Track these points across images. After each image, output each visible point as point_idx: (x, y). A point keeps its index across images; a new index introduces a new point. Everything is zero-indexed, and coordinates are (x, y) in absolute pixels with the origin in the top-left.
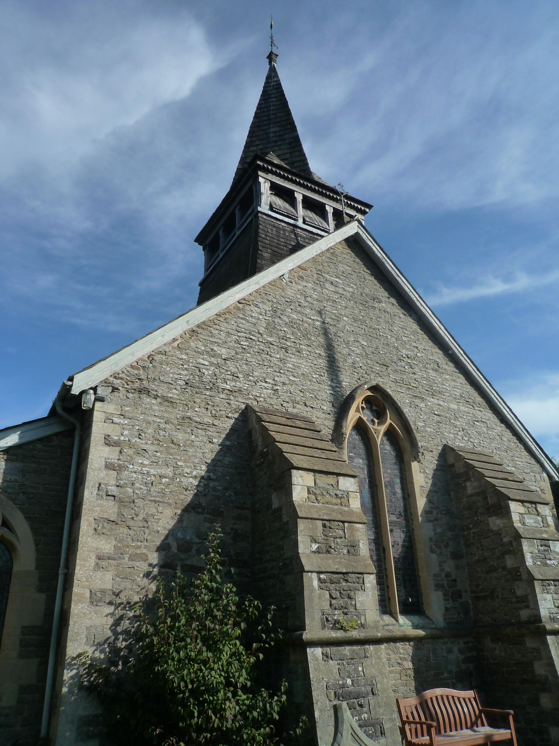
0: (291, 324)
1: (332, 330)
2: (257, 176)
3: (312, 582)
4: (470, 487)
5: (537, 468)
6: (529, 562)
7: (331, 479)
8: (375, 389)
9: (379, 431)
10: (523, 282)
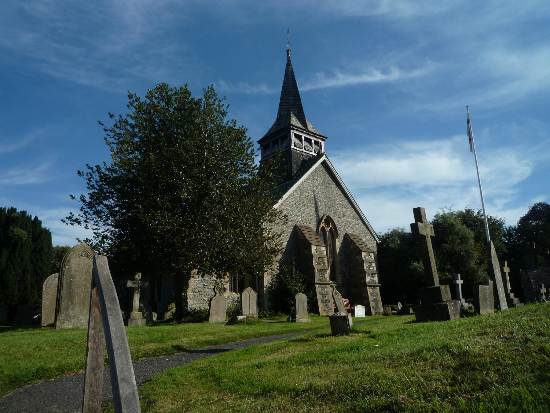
0: (306, 197)
1: (316, 197)
2: (290, 132)
3: (316, 271)
5: (373, 239)
6: (365, 268)
7: (319, 247)
8: (328, 217)
9: (328, 229)
10: (395, 75)
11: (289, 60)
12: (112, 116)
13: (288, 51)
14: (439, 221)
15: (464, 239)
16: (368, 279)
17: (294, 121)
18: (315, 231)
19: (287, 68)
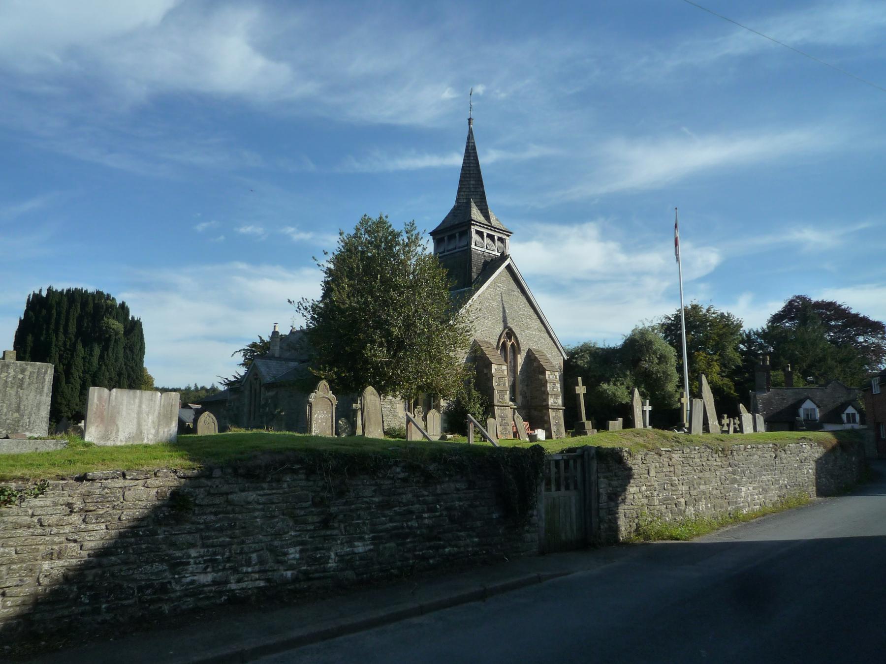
3: (496, 392)
4: (535, 364)
9: (509, 344)
11: (471, 131)
12: (326, 253)
13: (470, 120)
14: (636, 337)
15: (662, 359)
16: (551, 401)
17: (476, 214)
18: (495, 346)
19: (468, 143)
